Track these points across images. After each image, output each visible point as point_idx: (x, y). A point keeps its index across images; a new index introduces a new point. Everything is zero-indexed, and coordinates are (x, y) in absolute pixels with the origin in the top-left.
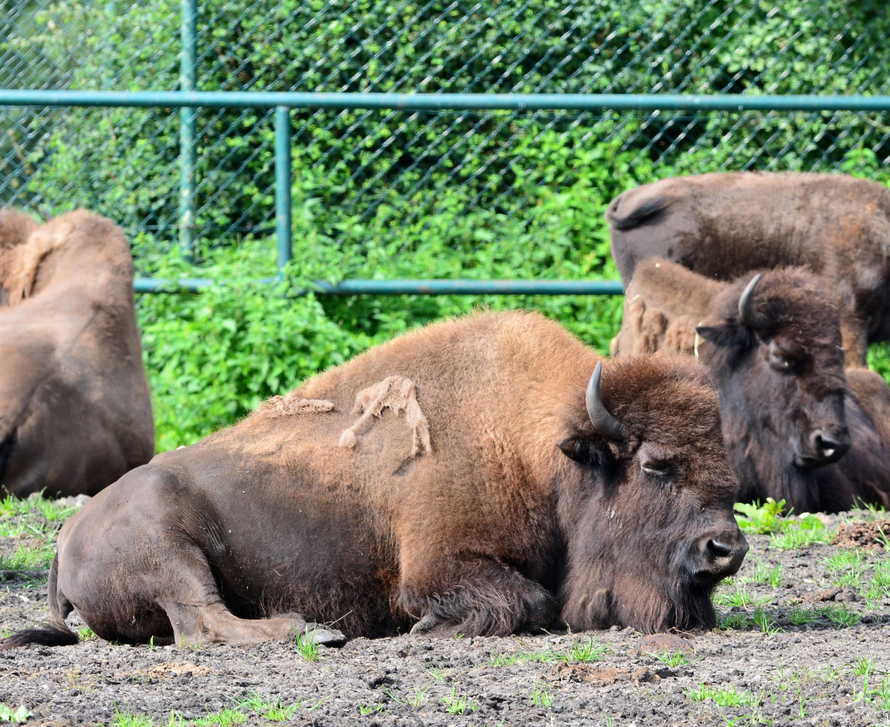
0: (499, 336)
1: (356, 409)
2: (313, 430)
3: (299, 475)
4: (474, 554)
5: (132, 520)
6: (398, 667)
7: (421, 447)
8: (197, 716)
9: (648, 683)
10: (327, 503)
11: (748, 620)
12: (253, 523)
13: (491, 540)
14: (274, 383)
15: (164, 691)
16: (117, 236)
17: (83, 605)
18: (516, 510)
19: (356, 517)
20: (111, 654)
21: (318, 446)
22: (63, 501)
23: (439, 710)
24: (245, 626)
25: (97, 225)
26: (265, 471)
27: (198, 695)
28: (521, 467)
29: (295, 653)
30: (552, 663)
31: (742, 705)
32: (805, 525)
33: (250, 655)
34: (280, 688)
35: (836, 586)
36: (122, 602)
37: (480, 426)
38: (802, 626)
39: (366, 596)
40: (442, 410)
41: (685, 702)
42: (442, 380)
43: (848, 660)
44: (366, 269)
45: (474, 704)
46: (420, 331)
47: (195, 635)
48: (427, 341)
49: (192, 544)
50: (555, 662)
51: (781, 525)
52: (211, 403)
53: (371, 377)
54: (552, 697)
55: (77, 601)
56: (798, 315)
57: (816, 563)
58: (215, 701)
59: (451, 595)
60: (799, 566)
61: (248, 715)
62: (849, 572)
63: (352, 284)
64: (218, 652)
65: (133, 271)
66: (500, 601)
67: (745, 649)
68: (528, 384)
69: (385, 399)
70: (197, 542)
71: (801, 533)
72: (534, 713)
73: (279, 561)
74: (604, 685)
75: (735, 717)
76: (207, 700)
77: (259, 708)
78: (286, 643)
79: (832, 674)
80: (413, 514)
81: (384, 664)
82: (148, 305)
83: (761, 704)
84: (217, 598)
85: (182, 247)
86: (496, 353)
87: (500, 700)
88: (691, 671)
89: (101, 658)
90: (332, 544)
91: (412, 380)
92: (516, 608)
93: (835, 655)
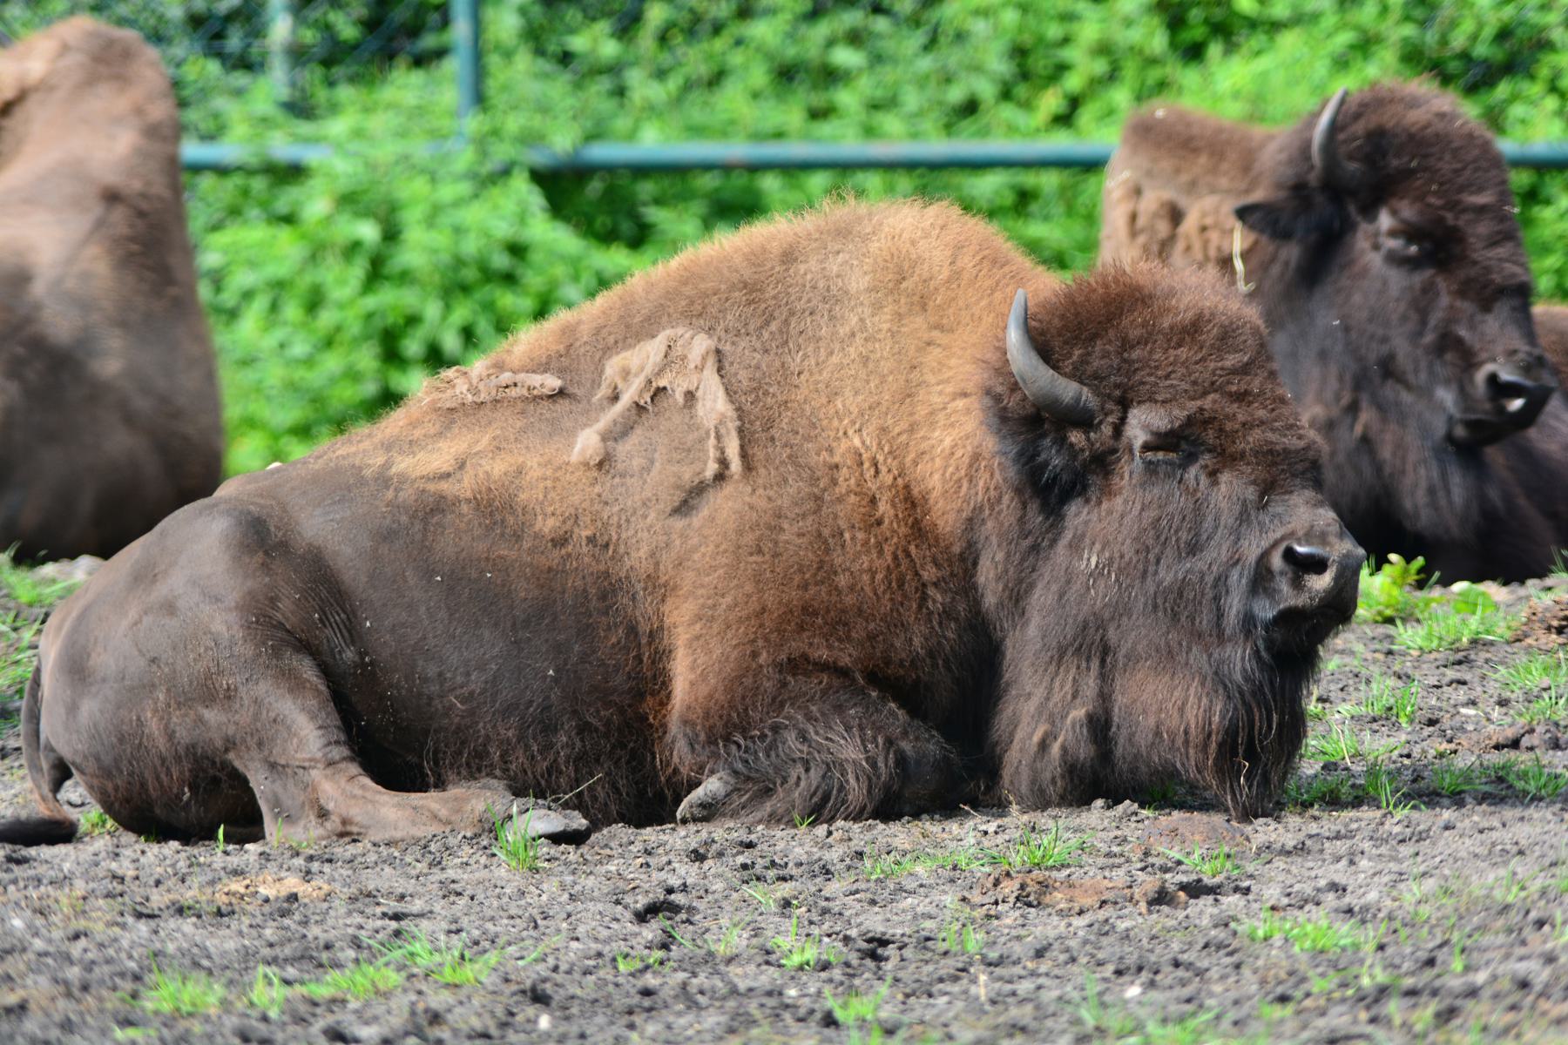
0: (874, 246)
1: (604, 391)
2: (523, 430)
3: (498, 517)
4: (815, 664)
5: (181, 604)
6: (690, 881)
7: (724, 463)
8: (306, 976)
9: (1165, 908)
10: (550, 569)
11: (1353, 786)
12: (411, 607)
13: (849, 638)
14: (451, 342)
15: (245, 930)
16: (151, 65)
17: (91, 766)
18: (901, 584)
19: (603, 597)
20: (143, 860)
21: (533, 462)
22: (49, 569)
23: (768, 963)
24: (398, 805)
25: (110, 43)
26: (433, 509)
27: (310, 937)
28: (911, 502)
29: (494, 855)
30: (981, 870)
31: (1344, 949)
32: (1461, 606)
33: (408, 859)
34: (464, 922)
35: (1522, 721)
36: (163, 760)
37: (836, 423)
38: (1457, 799)
39: (623, 746)
40: (766, 393)
41: (1235, 944)
42: (766, 335)
43: (1547, 861)
44: (622, 124)
45: (833, 950)
46: (730, 241)
47: (302, 823)
48: (738, 260)
49: (297, 650)
50: (987, 869)
51: (1416, 606)
52: (333, 381)
53: (635, 329)
54: (981, 936)
55: (78, 760)
56: (1426, 156)
57: (1483, 677)
58: (342, 949)
59: (763, 737)
60: (1449, 685)
61: (404, 974)
62: (1545, 695)
63: (601, 152)
64: (348, 855)
65: (178, 130)
66: (850, 751)
67: (1349, 843)
68: (926, 337)
69: (659, 373)
70: (305, 647)
71: (1454, 620)
72: (948, 966)
73: (459, 679)
74: (1081, 913)
75: (1331, 973)
76: (328, 947)
77: (425, 960)
78: (476, 836)
79: (1515, 889)
80: (702, 586)
81: (663, 876)
82: (208, 194)
83: (1381, 948)
84: (345, 751)
85: (273, 85)
86: (867, 278)
87: (884, 943)
88: (1246, 884)
89: (125, 867)
90: (558, 648)
91: (711, 336)
92: (881, 764)
93: (1521, 853)
